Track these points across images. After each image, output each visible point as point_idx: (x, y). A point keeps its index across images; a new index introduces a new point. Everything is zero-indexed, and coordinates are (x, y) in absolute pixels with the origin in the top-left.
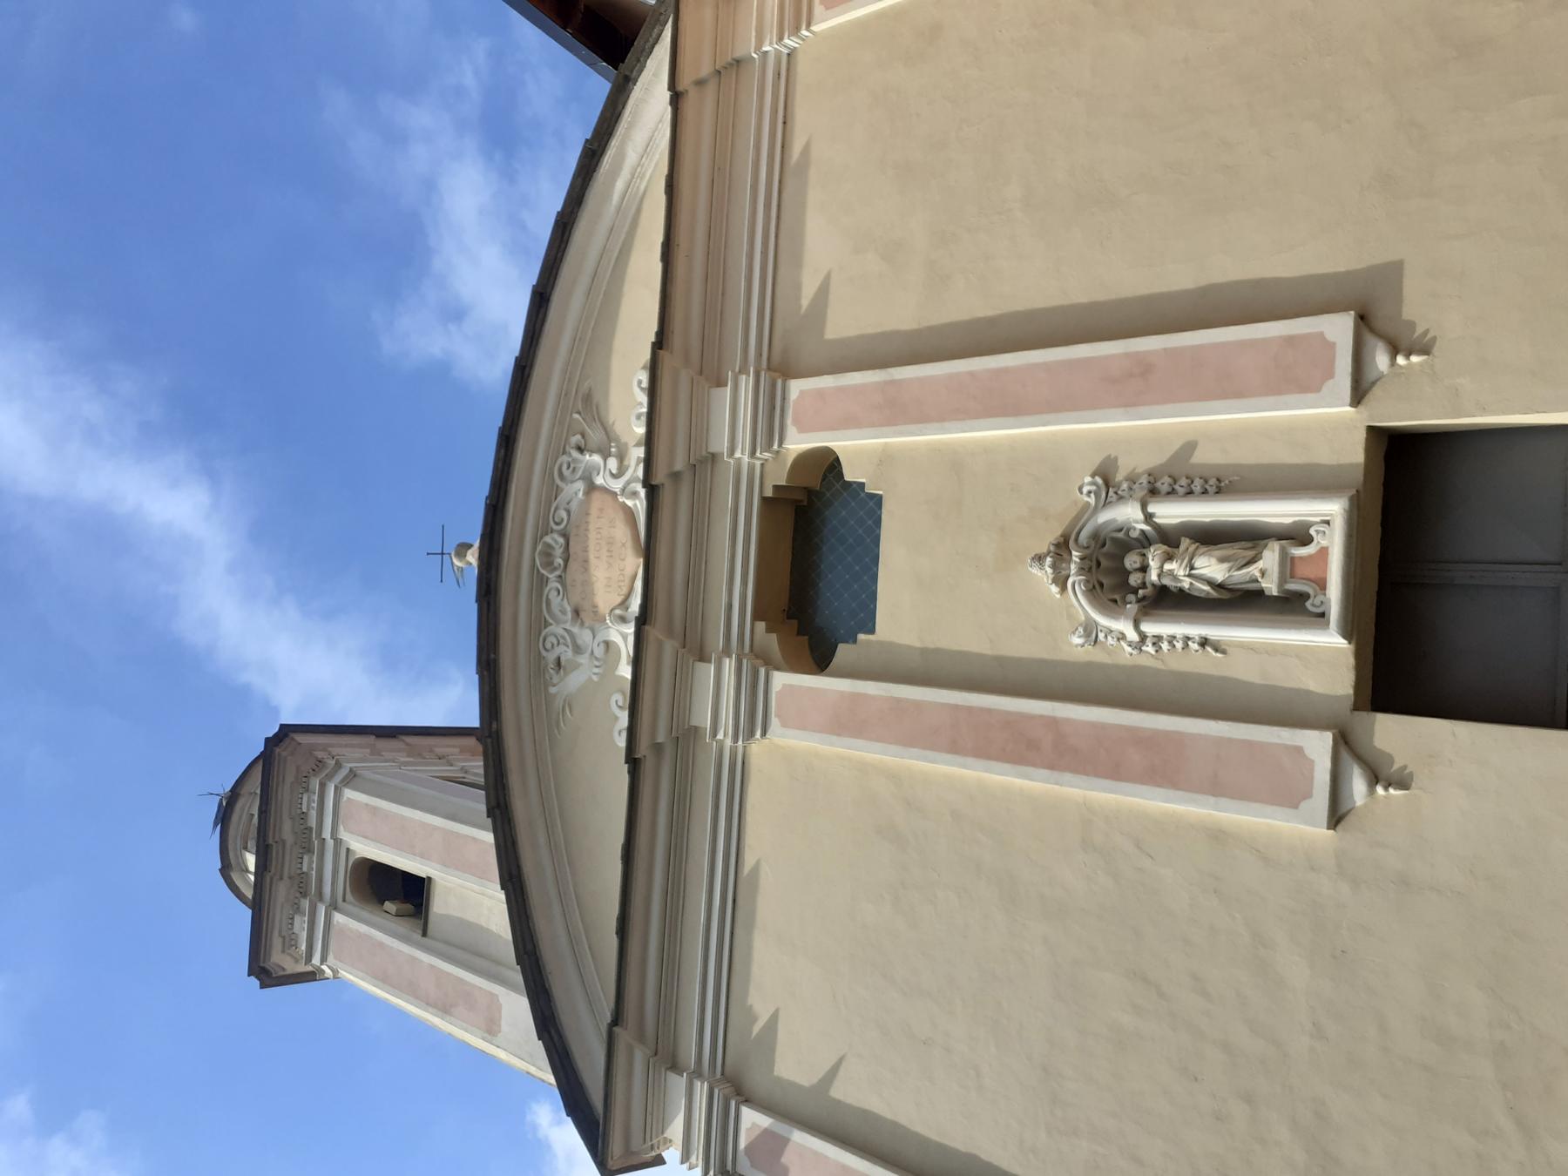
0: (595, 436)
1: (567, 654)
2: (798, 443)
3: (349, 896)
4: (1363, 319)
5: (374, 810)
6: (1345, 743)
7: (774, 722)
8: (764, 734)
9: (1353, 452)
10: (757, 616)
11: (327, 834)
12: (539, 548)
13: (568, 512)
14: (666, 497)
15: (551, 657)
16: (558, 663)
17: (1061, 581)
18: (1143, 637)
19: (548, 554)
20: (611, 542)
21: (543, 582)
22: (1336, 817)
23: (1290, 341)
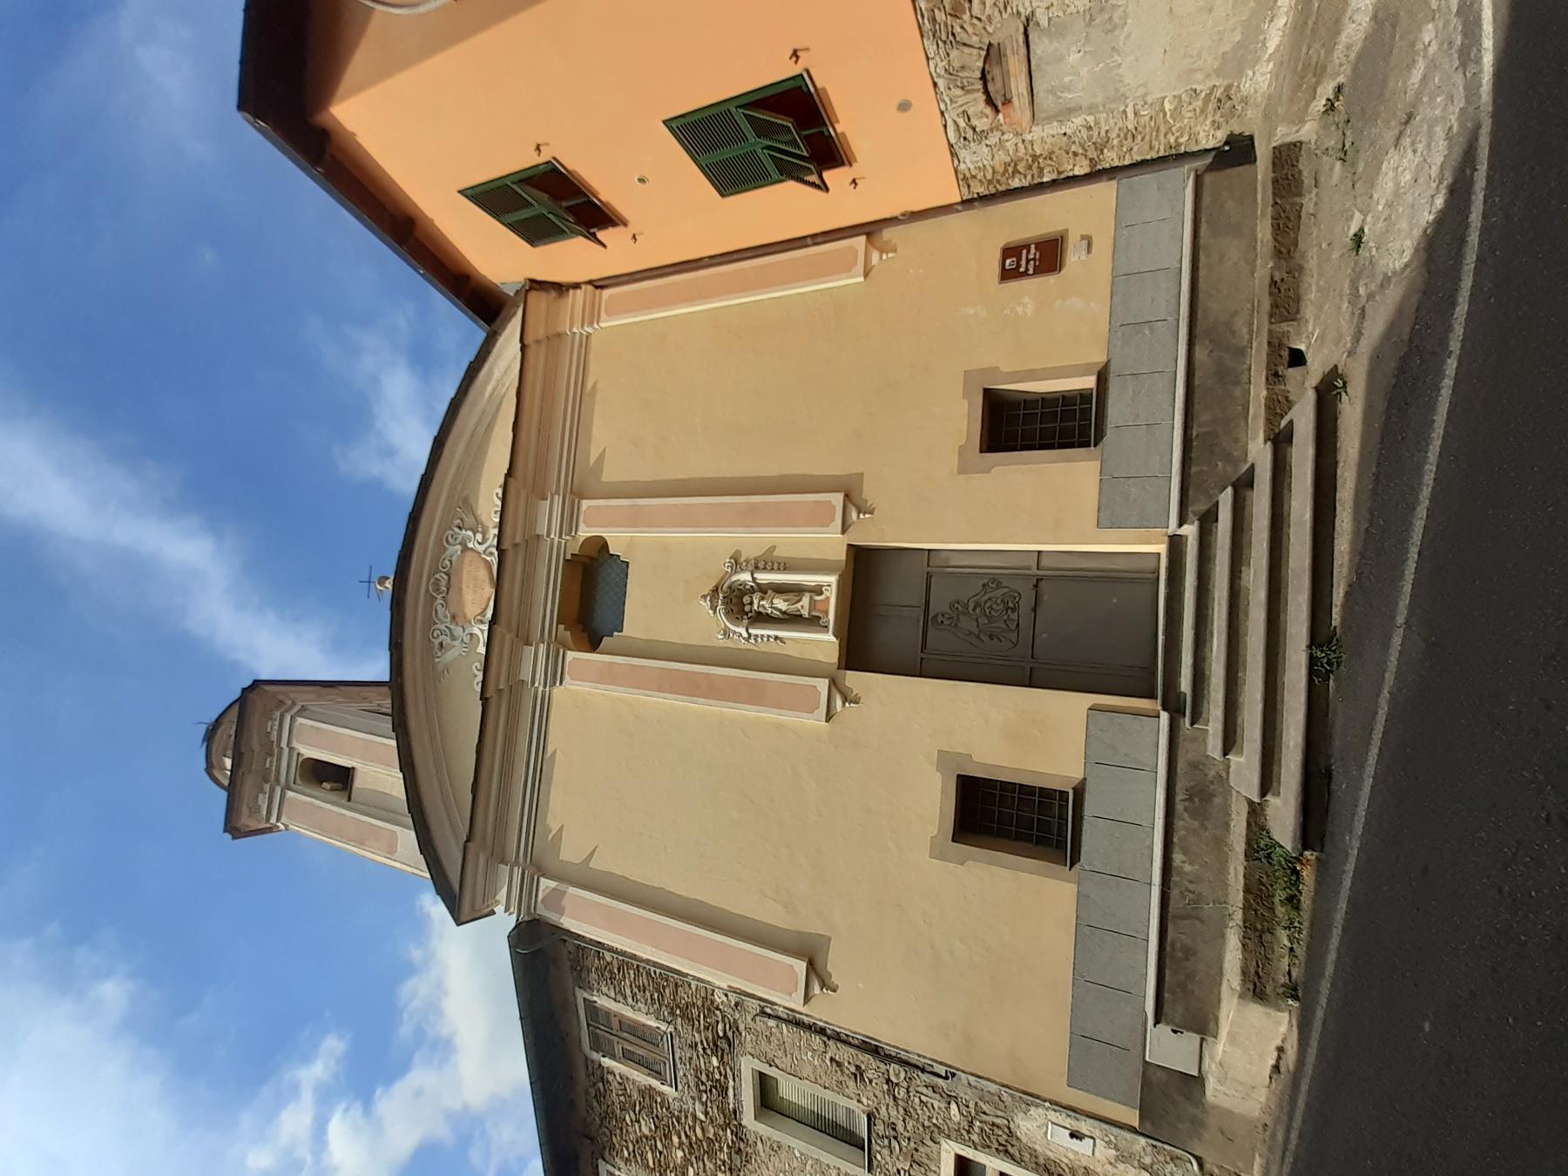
0: (469, 520)
1: (447, 640)
2: (585, 532)
3: (298, 781)
6: (834, 683)
7: (567, 678)
8: (561, 684)
9: (842, 555)
11: (284, 744)
12: (432, 580)
13: (451, 562)
14: (509, 556)
15: (436, 642)
16: (441, 644)
18: (750, 635)
19: (437, 583)
20: (476, 579)
21: (434, 599)
22: (829, 717)
23: (817, 502)
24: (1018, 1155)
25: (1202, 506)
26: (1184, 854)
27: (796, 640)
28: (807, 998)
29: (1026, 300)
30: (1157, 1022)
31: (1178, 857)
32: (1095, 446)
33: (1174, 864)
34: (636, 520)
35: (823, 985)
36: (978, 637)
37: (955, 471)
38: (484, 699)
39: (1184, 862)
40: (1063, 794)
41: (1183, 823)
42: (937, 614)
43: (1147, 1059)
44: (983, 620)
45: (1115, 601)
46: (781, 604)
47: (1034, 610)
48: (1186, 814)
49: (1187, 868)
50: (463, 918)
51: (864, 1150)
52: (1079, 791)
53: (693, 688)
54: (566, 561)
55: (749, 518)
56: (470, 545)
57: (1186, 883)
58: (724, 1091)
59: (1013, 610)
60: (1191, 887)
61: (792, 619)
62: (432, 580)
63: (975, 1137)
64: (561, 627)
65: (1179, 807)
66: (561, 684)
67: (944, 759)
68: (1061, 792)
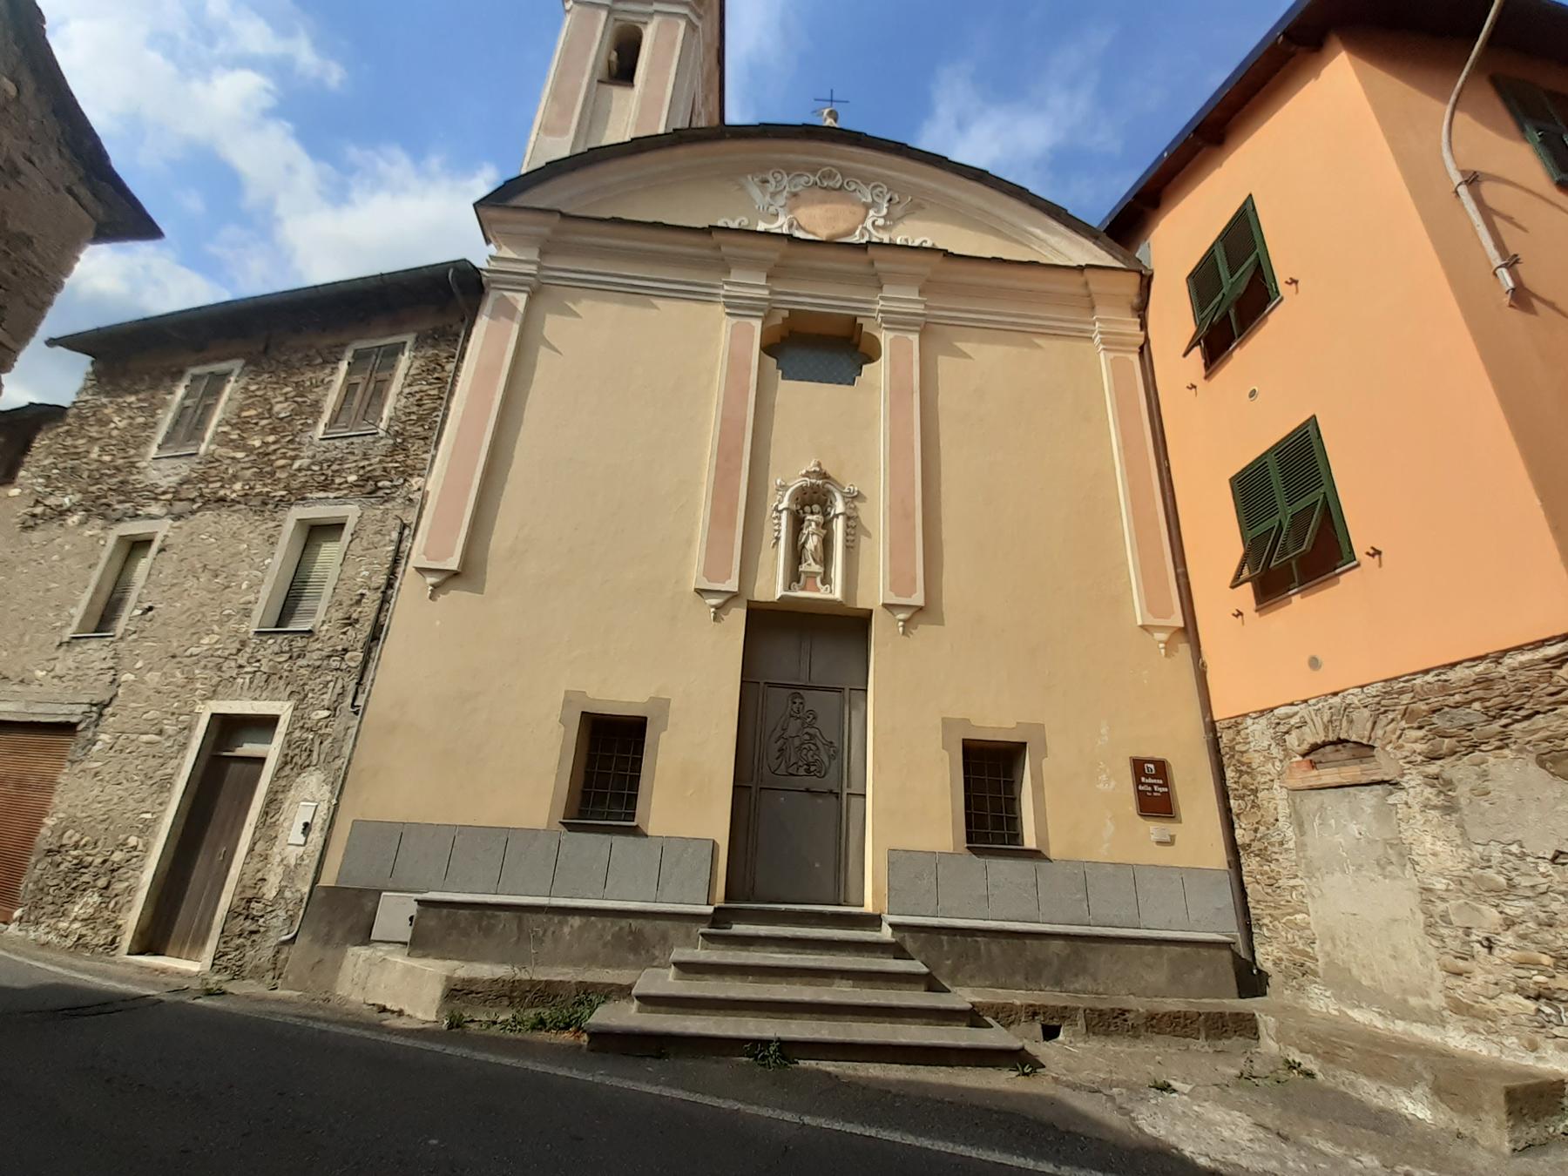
1: (771, 187)
2: (885, 338)
3: (618, 24)
4: (921, 609)
5: (673, 44)
6: (733, 597)
7: (734, 320)
9: (862, 603)
10: (791, 311)
12: (834, 170)
17: (808, 474)
18: (781, 512)
19: (830, 176)
21: (814, 172)
22: (700, 591)
24: (284, 774)
25: (910, 945)
26: (580, 927)
27: (775, 563)
28: (421, 570)
29: (1113, 783)
30: (420, 902)
31: (576, 921)
32: (968, 848)
33: (569, 918)
34: (898, 394)
35: (435, 587)
36: (780, 737)
37: (945, 716)
38: (712, 229)
39: (572, 926)
40: (632, 817)
41: (611, 927)
42: (802, 698)
43: (384, 894)
44: (797, 742)
45: (817, 865)
46: (812, 543)
47: (807, 790)
48: (617, 928)
49: (566, 930)
50: (481, 210)
51: (277, 627)
52: (636, 832)
53: (726, 455)
54: (855, 318)
55: (899, 513)
56: (871, 212)
57: (552, 929)
58: (324, 487)
59: (808, 771)
60: (549, 933)
61: (797, 554)
62: (834, 170)
63: (297, 734)
64: (786, 314)
65: (624, 923)
66: (728, 314)
67: (663, 705)
68: (634, 815)
